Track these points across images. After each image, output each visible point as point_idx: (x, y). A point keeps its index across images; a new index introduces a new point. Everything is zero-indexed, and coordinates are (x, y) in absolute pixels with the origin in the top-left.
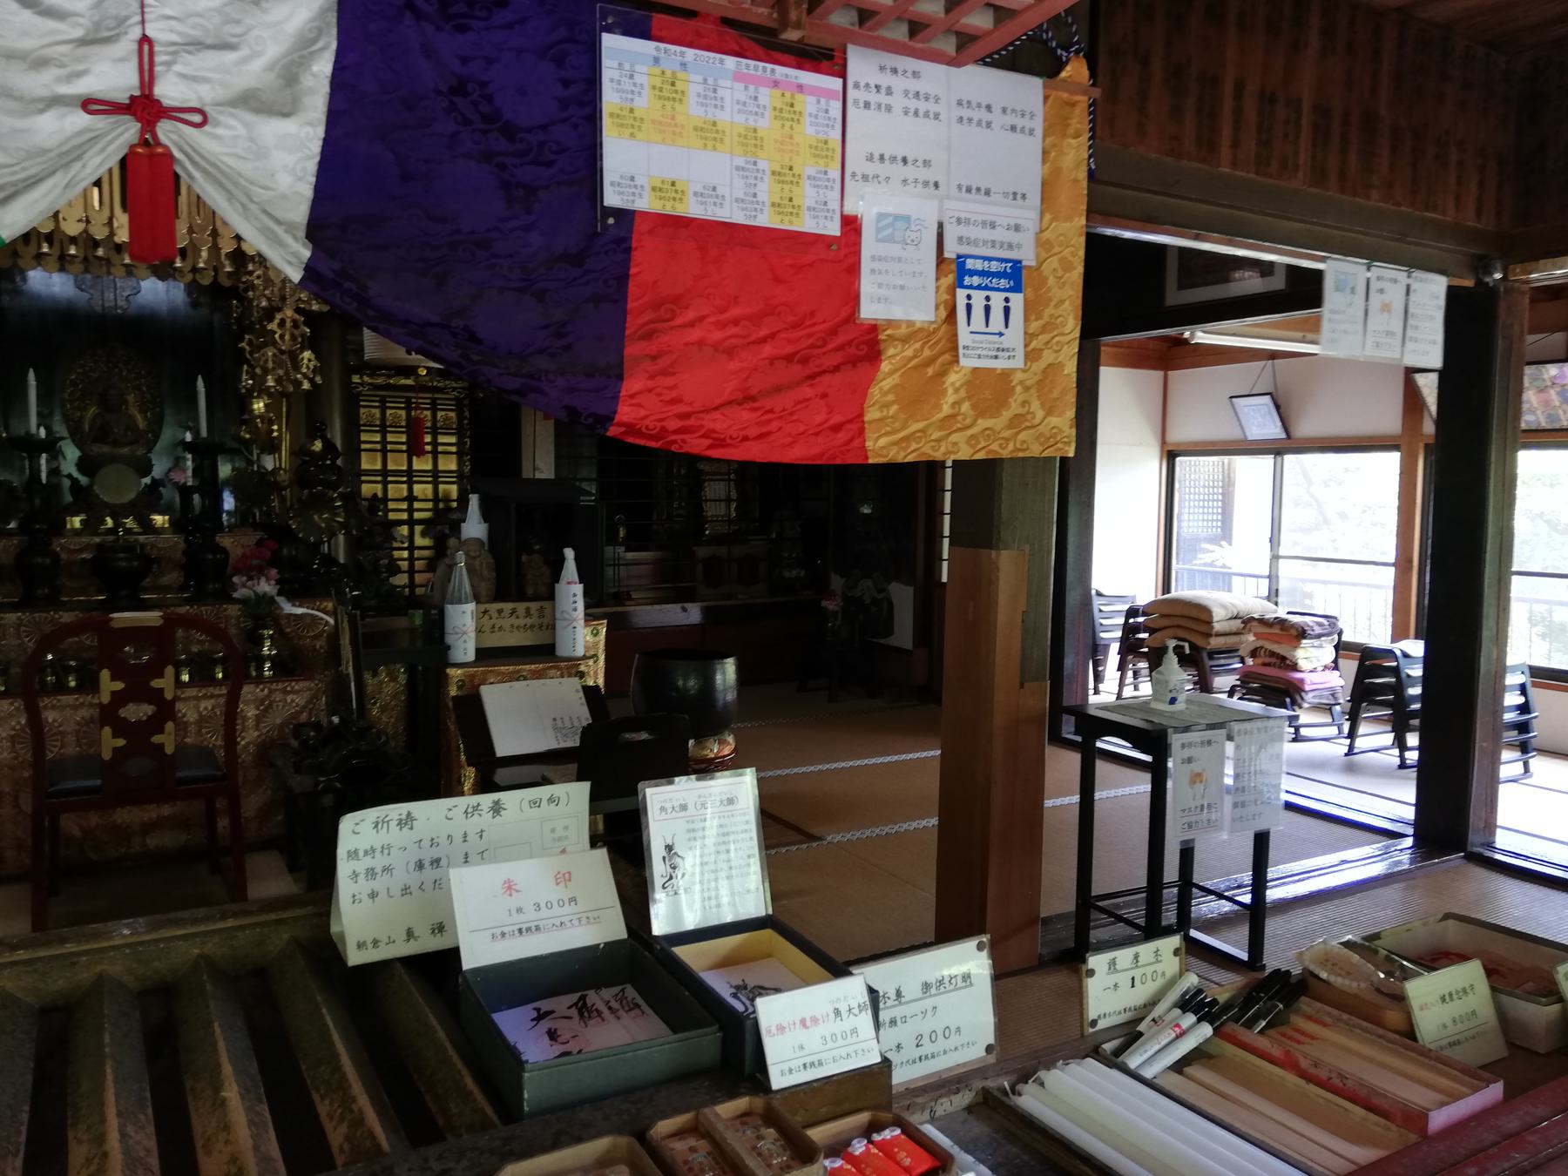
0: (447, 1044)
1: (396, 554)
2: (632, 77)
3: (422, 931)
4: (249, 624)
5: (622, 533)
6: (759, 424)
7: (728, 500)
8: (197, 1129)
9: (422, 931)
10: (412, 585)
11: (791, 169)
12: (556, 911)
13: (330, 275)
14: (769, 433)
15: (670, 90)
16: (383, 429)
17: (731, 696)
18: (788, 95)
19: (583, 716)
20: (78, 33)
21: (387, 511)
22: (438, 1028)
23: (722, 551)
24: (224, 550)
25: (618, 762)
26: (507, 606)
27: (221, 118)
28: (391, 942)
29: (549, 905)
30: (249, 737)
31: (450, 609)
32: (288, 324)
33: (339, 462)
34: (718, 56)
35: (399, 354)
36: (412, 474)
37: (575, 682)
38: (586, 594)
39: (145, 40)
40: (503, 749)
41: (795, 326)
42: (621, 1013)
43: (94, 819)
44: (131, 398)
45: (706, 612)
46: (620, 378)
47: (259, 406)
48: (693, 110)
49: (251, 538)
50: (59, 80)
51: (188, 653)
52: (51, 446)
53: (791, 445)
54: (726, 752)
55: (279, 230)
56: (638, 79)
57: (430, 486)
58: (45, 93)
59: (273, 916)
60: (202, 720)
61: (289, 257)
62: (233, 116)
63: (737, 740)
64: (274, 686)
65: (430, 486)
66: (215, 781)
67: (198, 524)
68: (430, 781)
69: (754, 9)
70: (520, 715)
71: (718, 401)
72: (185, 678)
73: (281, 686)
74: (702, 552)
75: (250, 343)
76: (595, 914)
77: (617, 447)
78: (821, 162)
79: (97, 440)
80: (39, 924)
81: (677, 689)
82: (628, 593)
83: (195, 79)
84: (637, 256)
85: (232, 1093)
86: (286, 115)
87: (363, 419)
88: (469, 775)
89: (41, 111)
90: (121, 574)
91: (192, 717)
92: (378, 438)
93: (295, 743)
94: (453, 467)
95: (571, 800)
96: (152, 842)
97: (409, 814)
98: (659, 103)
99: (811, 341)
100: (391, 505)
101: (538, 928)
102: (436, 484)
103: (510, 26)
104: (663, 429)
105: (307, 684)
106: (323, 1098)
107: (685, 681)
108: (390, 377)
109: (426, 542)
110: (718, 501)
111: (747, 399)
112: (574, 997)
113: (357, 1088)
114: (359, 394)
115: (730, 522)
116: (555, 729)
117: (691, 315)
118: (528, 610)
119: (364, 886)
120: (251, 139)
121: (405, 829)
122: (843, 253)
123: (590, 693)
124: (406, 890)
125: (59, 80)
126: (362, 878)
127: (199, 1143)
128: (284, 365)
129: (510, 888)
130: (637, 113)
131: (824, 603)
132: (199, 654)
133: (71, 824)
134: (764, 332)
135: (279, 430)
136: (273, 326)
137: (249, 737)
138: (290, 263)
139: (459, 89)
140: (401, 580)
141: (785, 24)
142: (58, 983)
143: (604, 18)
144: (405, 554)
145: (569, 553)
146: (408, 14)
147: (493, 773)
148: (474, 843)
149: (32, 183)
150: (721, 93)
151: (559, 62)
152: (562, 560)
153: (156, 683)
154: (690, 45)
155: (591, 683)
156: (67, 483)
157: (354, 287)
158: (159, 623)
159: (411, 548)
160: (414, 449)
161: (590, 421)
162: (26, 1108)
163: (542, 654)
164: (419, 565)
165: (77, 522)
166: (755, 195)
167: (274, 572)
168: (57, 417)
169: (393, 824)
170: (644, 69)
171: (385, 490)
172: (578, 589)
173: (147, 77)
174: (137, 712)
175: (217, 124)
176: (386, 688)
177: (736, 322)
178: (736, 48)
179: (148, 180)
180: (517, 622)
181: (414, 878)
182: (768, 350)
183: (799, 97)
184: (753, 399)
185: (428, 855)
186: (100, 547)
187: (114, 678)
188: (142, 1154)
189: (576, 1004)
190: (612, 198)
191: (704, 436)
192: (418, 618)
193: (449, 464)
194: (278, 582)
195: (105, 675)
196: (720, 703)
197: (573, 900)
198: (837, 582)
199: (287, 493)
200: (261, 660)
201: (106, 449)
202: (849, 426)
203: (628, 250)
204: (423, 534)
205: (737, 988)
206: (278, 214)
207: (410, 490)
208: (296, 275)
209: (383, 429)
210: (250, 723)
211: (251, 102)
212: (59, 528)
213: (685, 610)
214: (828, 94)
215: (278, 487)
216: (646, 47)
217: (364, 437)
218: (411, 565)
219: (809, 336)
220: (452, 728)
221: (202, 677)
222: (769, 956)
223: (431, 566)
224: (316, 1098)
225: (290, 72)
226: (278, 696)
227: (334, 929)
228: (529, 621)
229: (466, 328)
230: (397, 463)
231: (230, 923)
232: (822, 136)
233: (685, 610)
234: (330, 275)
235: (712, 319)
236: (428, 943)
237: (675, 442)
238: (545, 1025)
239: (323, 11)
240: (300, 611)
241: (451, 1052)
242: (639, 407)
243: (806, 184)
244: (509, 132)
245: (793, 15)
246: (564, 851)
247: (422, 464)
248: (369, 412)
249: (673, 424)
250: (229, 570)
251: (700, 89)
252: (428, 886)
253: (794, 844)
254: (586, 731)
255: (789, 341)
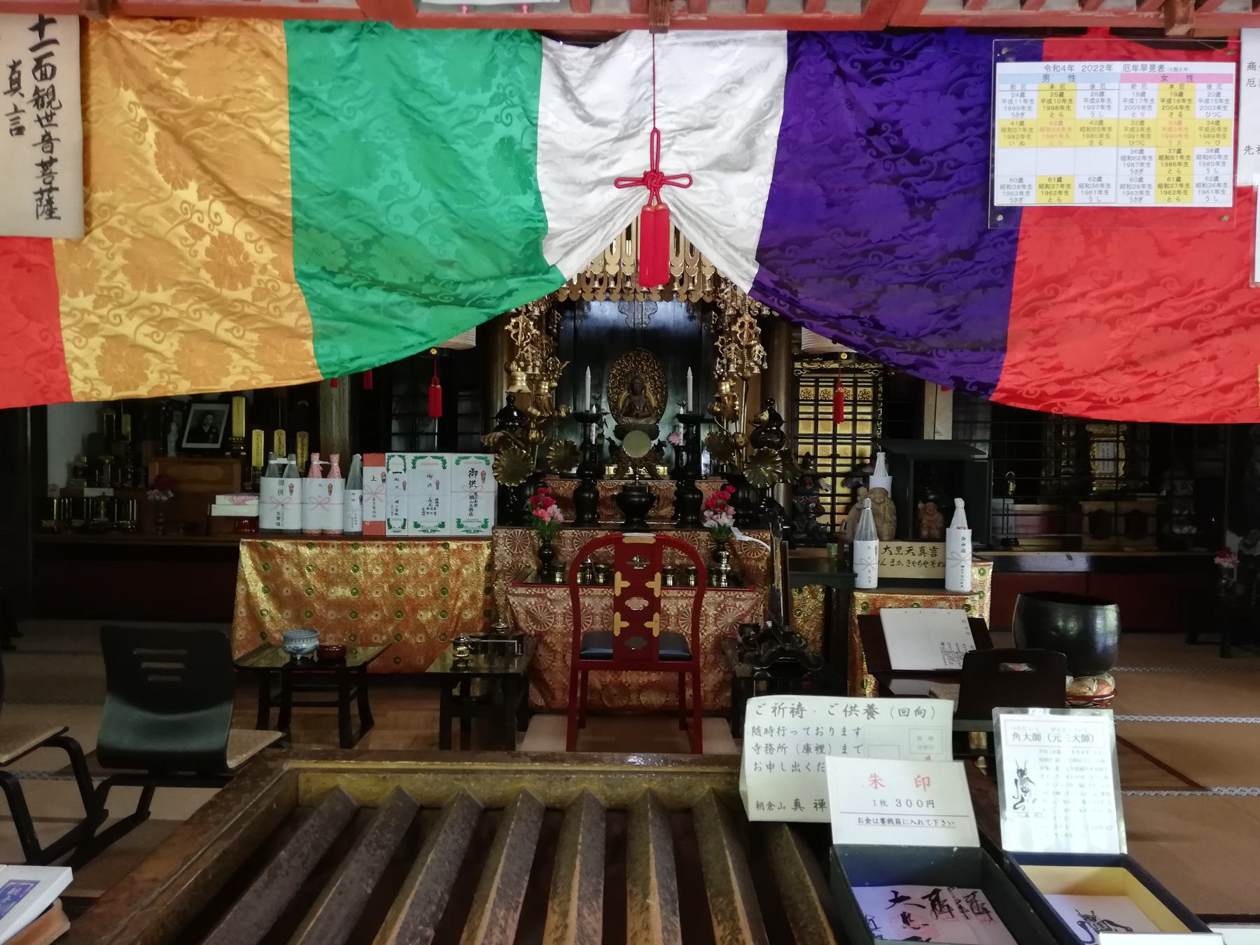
0: (818, 904)
1: (822, 499)
2: (1023, 95)
3: (808, 804)
4: (714, 546)
5: (1012, 487)
6: (1141, 387)
7: (1116, 460)
8: (630, 925)
9: (808, 804)
10: (833, 524)
11: (1179, 151)
12: (915, 809)
13: (771, 285)
14: (1152, 395)
15: (1059, 100)
16: (816, 403)
17: (1112, 640)
18: (1177, 86)
19: (969, 644)
20: (615, 134)
21: (816, 465)
22: (812, 888)
23: (1109, 506)
24: (700, 492)
25: (988, 684)
26: (905, 545)
27: (702, 179)
28: (782, 807)
29: (909, 803)
30: (709, 630)
31: (857, 543)
32: (746, 326)
33: (782, 428)
34: (1105, 63)
35: (827, 345)
36: (838, 433)
37: (962, 615)
38: (974, 539)
39: (655, 131)
40: (897, 663)
41: (1181, 295)
42: (970, 914)
43: (609, 677)
44: (648, 385)
45: (1093, 561)
46: (1004, 350)
47: (726, 387)
48: (1081, 113)
49: (718, 484)
50: (602, 168)
51: (672, 564)
52: (598, 419)
53: (1175, 406)
54: (1105, 692)
55: (737, 256)
56: (1028, 96)
57: (849, 447)
58: (594, 178)
59: (698, 769)
60: (679, 614)
61: (742, 274)
62: (709, 176)
63: (1116, 680)
64: (728, 594)
65: (849, 447)
66: (683, 660)
67: (685, 473)
68: (836, 682)
69: (1140, 14)
70: (920, 636)
71: (1097, 368)
72: (670, 582)
73: (732, 594)
74: (1089, 507)
75: (723, 342)
76: (950, 819)
77: (999, 410)
78: (1213, 141)
79: (626, 415)
80: (571, 746)
81: (1056, 629)
82: (1016, 540)
83: (686, 154)
84: (1023, 245)
85: (654, 901)
86: (745, 170)
87: (802, 396)
88: (870, 681)
89: (591, 191)
90: (635, 508)
91: (672, 611)
92: (812, 409)
93: (740, 639)
94: (869, 431)
95: (939, 713)
96: (644, 699)
97: (800, 705)
98: (1166, 169)
99: (1199, 307)
100: (820, 461)
101: (898, 822)
102: (854, 445)
103: (919, 73)
104: (1044, 394)
105: (750, 594)
106: (719, 923)
107: (1065, 621)
108: (822, 362)
109: (846, 490)
110: (1106, 459)
111: (1129, 363)
112: (930, 889)
113: (743, 922)
114: (800, 376)
115: (1118, 479)
116: (943, 652)
117: (1072, 292)
118: (922, 549)
119: (764, 758)
120: (721, 192)
121: (796, 717)
122: (1235, 222)
123: (976, 624)
124: (795, 767)
125: (602, 168)
126: (762, 751)
127: (629, 935)
128: (743, 355)
129: (875, 781)
130: (1027, 125)
131: (1218, 560)
132: (681, 566)
133: (595, 678)
134: (1147, 303)
135: (740, 405)
136: (735, 328)
137: (709, 630)
138: (743, 279)
139: (875, 130)
140: (824, 520)
141: (1171, 21)
142: (558, 791)
143: (999, 50)
144: (829, 499)
145: (960, 503)
146: (838, 78)
147: (889, 682)
148: (851, 739)
149: (582, 240)
150: (1107, 94)
151: (959, 95)
152: (952, 508)
153: (649, 585)
154: (1080, 58)
155: (977, 616)
156: (607, 443)
157: (788, 294)
158: (653, 541)
159: (833, 495)
160: (838, 418)
161: (975, 388)
162: (527, 878)
163: (933, 586)
164: (839, 508)
165: (611, 470)
166: (1141, 180)
167: (731, 509)
168: (604, 399)
169: (787, 711)
170: (1035, 87)
171: (816, 450)
172: (968, 533)
173: (655, 157)
174: (637, 604)
175: (698, 184)
176: (808, 604)
177: (1119, 295)
178: (1124, 53)
179: (655, 230)
180: (912, 559)
181: (803, 759)
182: (1152, 318)
183: (1188, 86)
184: (1135, 364)
185: (814, 741)
186: (624, 487)
187: (623, 579)
188: (591, 932)
189: (929, 896)
190: (1001, 199)
191: (1085, 399)
192: (834, 549)
193: (865, 429)
194: (734, 517)
195: (618, 575)
196: (1100, 646)
197: (930, 803)
198: (1233, 541)
199: (743, 451)
200: (720, 573)
201: (631, 420)
202: (1241, 387)
203: (1016, 240)
204: (843, 485)
205: (1086, 917)
206: (738, 245)
207: (834, 449)
208: (746, 287)
209: (816, 403)
210: (711, 620)
211: (724, 164)
212: (600, 474)
213: (1070, 558)
214: (1221, 79)
215: (737, 447)
216: (1037, 67)
217: (802, 409)
218: (833, 509)
219: (1197, 303)
220: (857, 640)
221: (681, 583)
222: (1122, 893)
223: (848, 507)
224: (715, 923)
225: (749, 140)
226: (730, 602)
227: (742, 788)
228: (922, 558)
229: (872, 318)
230: (825, 428)
231: (670, 769)
232: (1213, 118)
233: (1070, 558)
234: (771, 285)
235: (1094, 294)
236: (809, 815)
237: (1055, 405)
238: (901, 908)
239: (773, 92)
240: (747, 539)
241: (820, 911)
242: (1021, 375)
243: (1195, 164)
244: (914, 157)
245: (1180, 12)
246: (928, 759)
247: (844, 429)
248: (806, 391)
249: (1052, 389)
250: (703, 506)
251: (1088, 95)
252: (813, 767)
253: (1176, 789)
254: (968, 657)
255: (1175, 309)
